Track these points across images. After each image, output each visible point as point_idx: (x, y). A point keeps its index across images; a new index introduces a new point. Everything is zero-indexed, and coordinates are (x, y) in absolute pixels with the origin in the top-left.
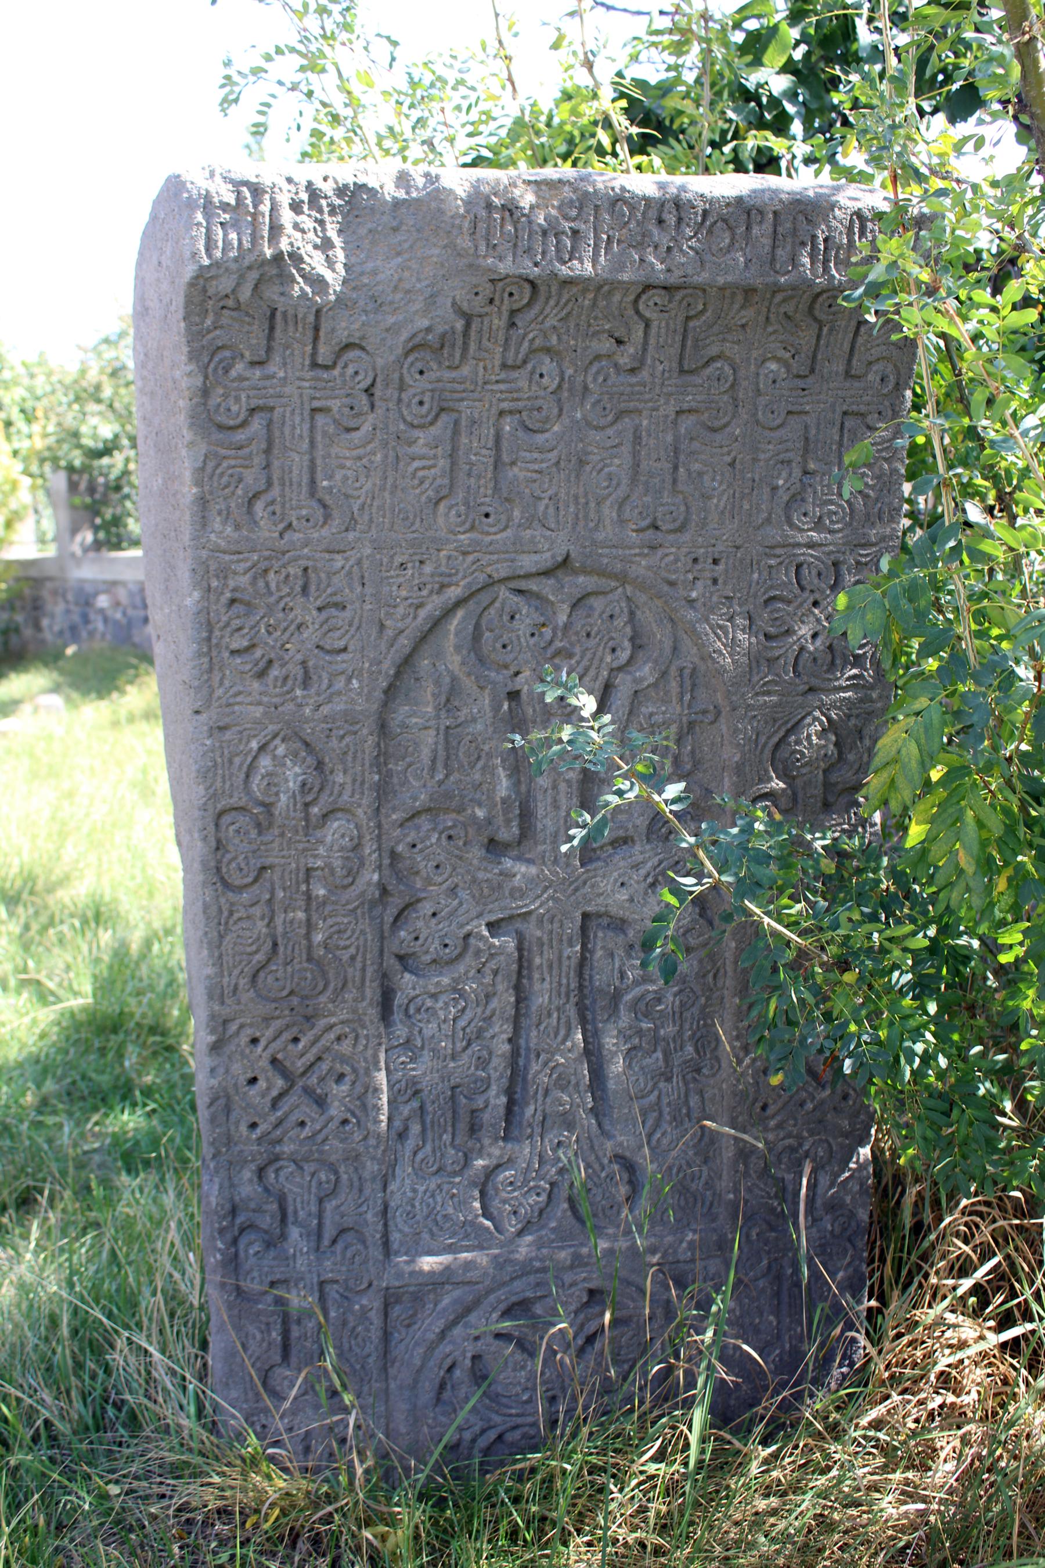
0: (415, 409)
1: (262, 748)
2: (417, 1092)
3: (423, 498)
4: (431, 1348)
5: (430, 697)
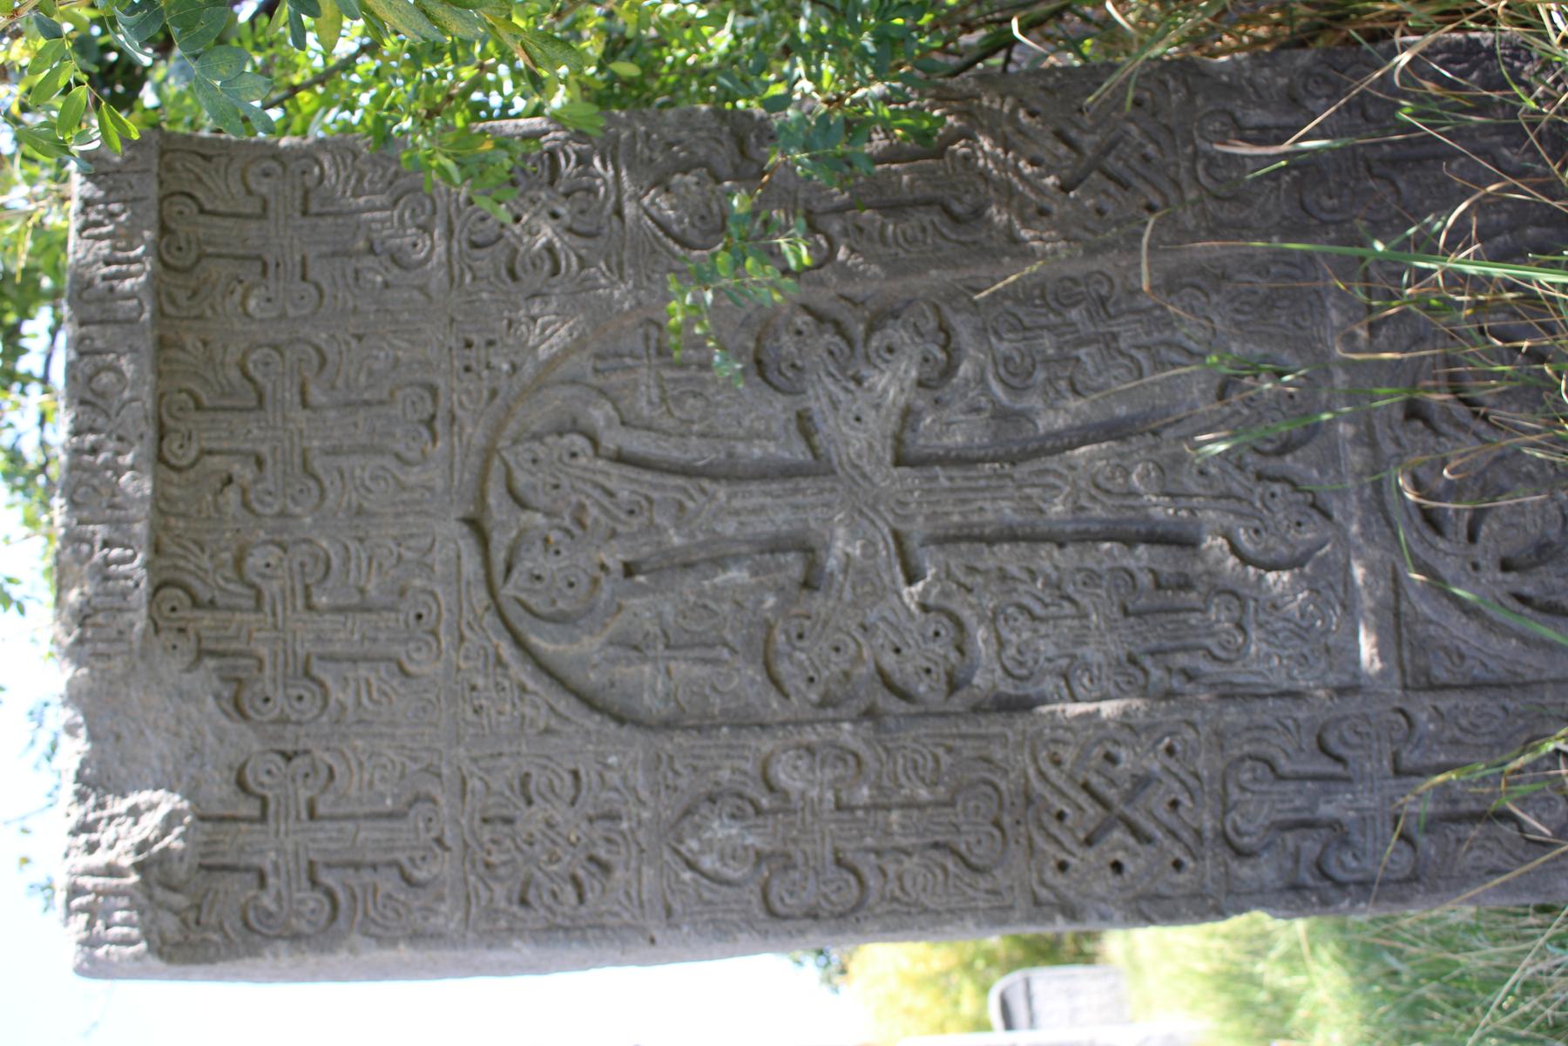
0: (305, 705)
1: (691, 866)
2: (1132, 660)
3: (402, 690)
4: (1491, 626)
5: (632, 670)
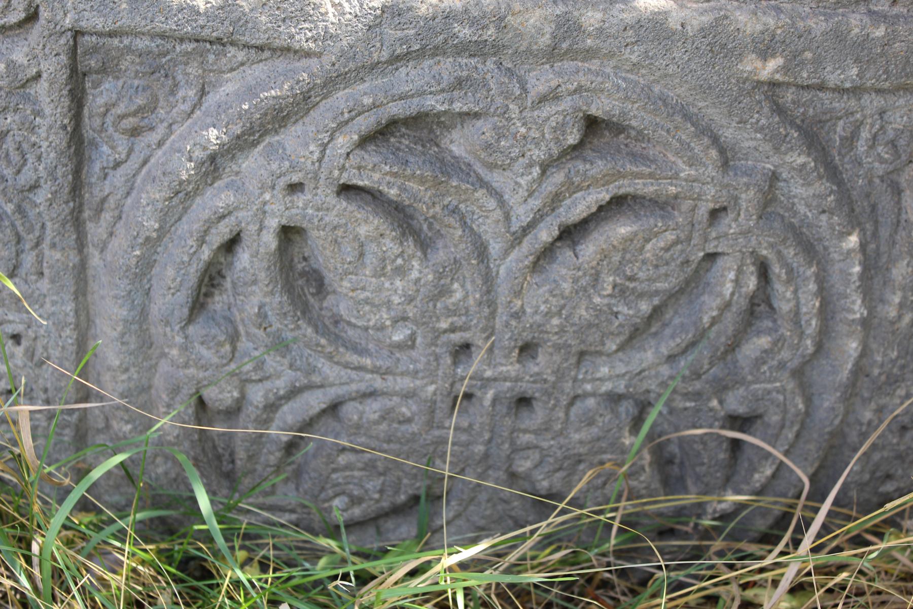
4: (184, 195)
